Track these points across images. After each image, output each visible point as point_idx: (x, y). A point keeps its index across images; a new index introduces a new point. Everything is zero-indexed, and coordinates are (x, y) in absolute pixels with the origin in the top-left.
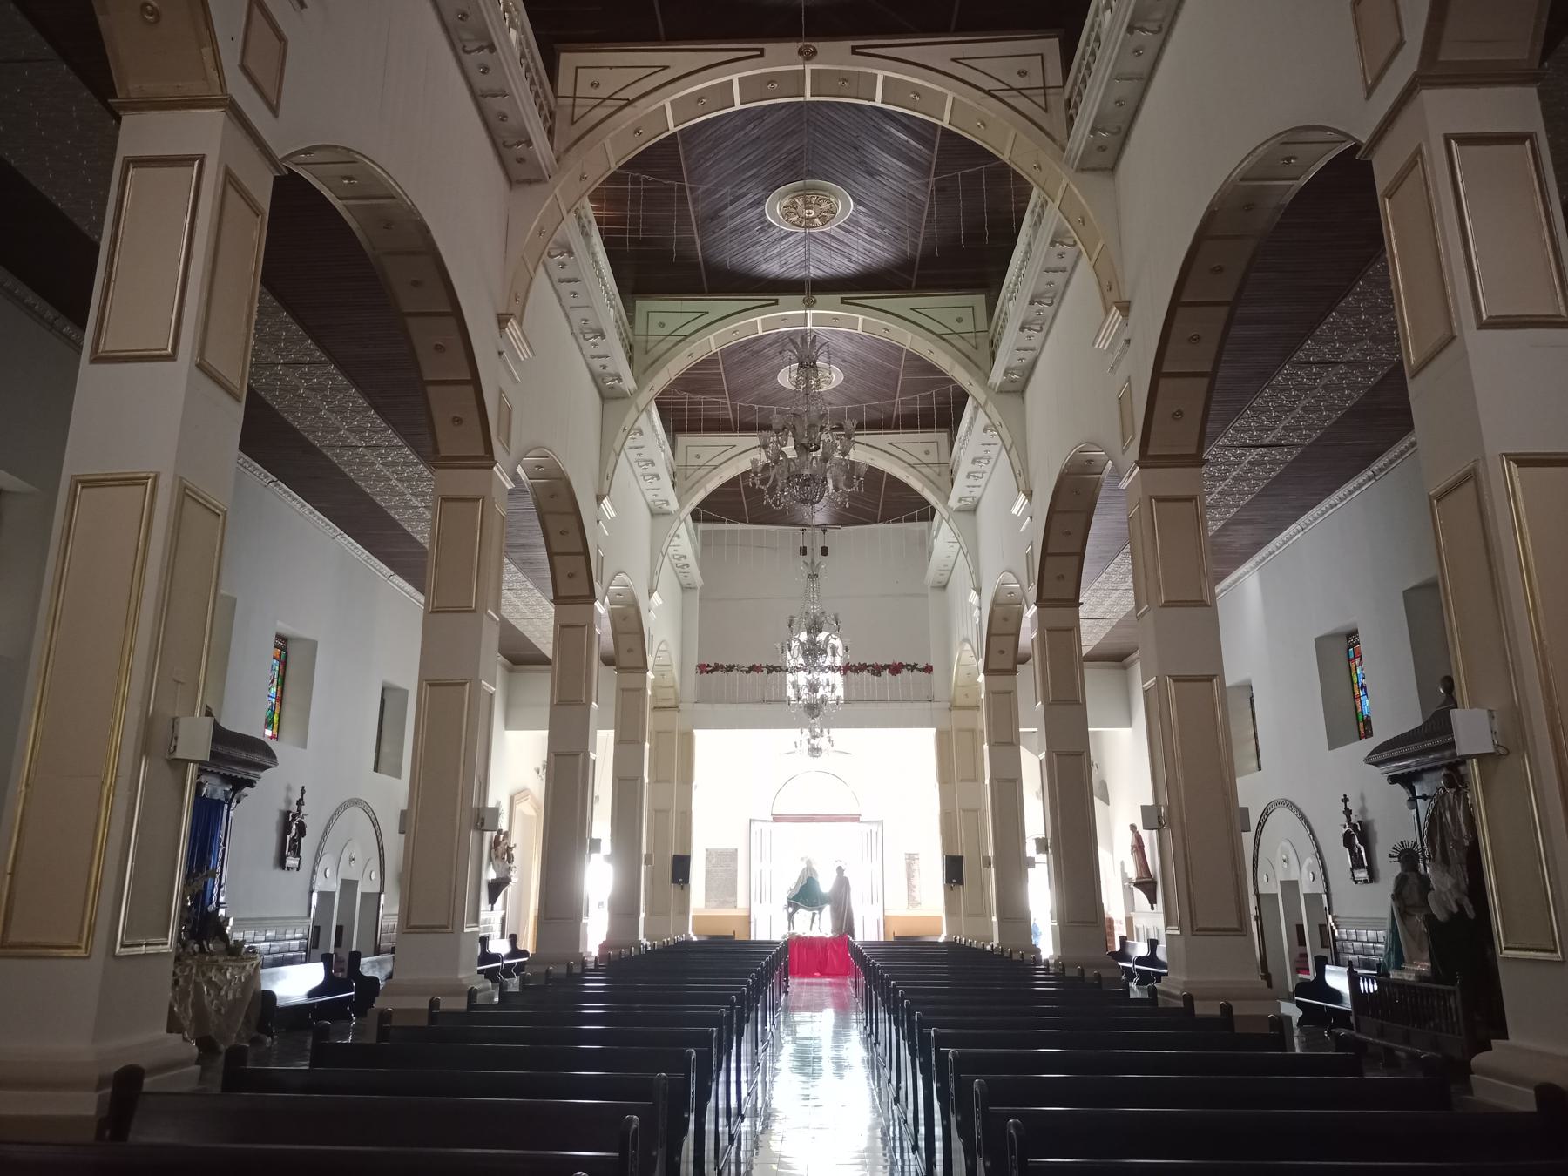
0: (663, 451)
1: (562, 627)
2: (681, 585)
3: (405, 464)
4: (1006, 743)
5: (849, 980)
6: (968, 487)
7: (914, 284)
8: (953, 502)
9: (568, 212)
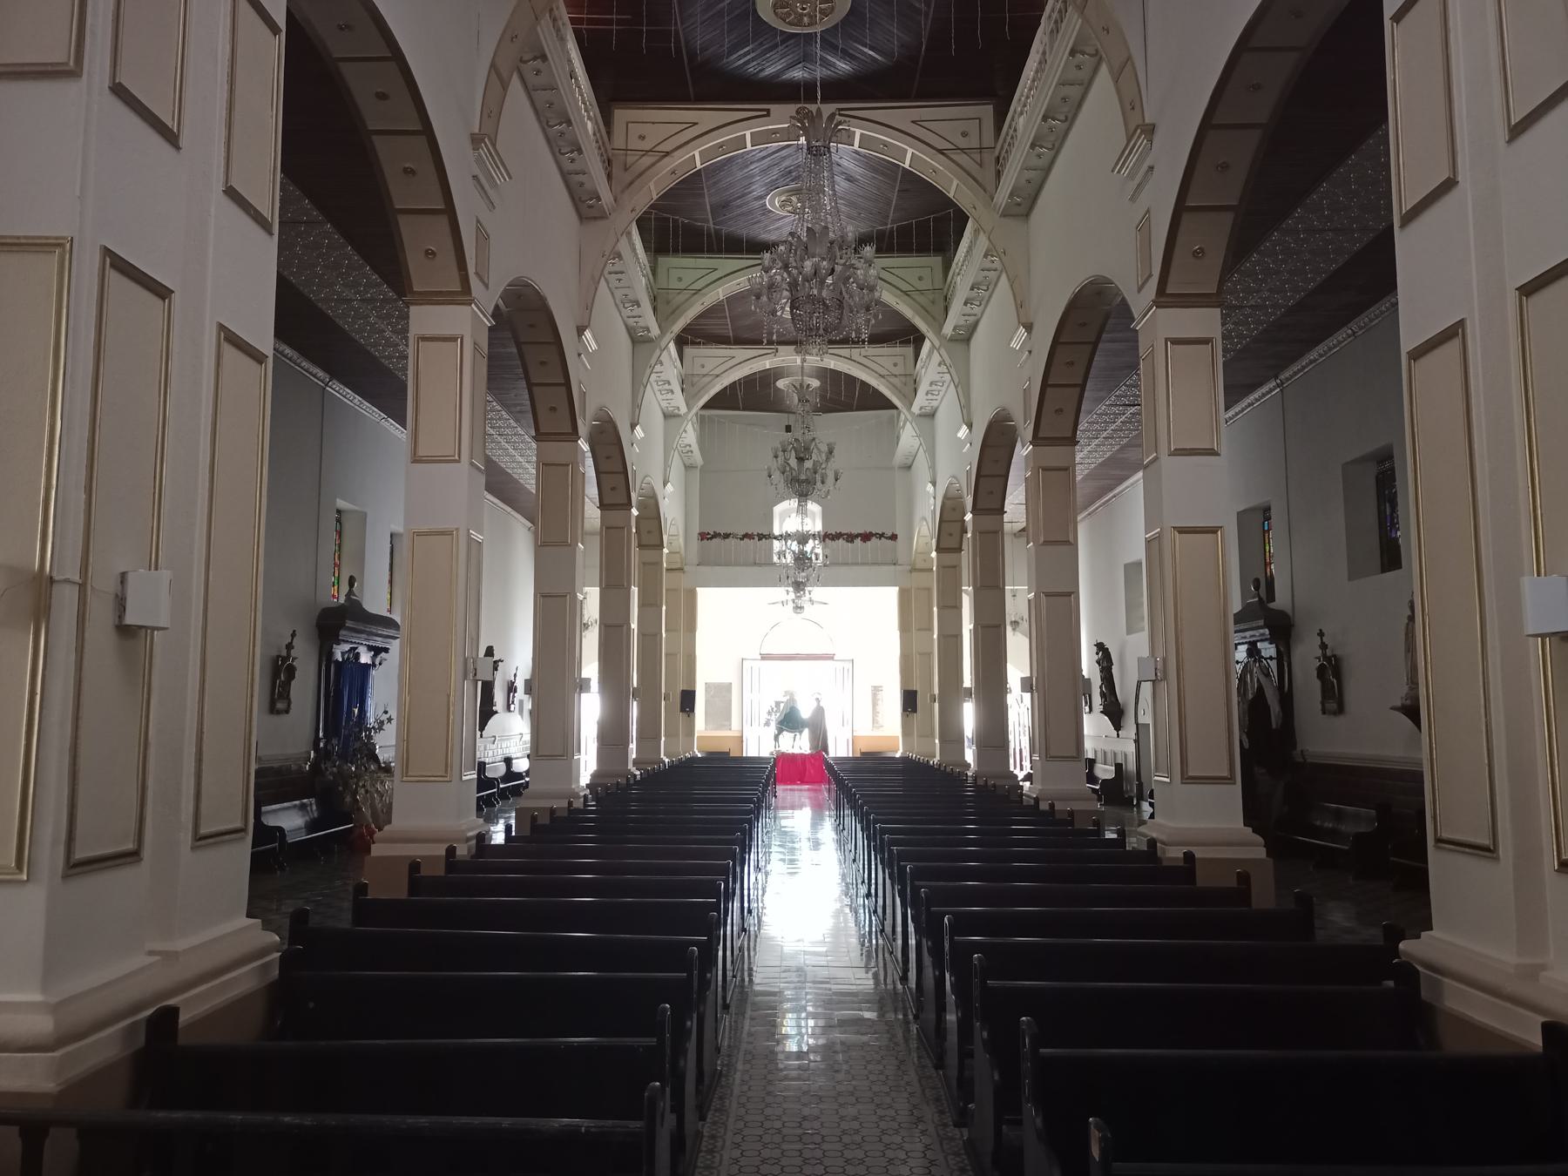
0: (675, 367)
1: (607, 528)
2: (684, 464)
3: (386, 301)
4: (951, 607)
5: (824, 787)
6: (964, 315)
7: (884, 248)
8: (915, 409)
9: (622, 235)
